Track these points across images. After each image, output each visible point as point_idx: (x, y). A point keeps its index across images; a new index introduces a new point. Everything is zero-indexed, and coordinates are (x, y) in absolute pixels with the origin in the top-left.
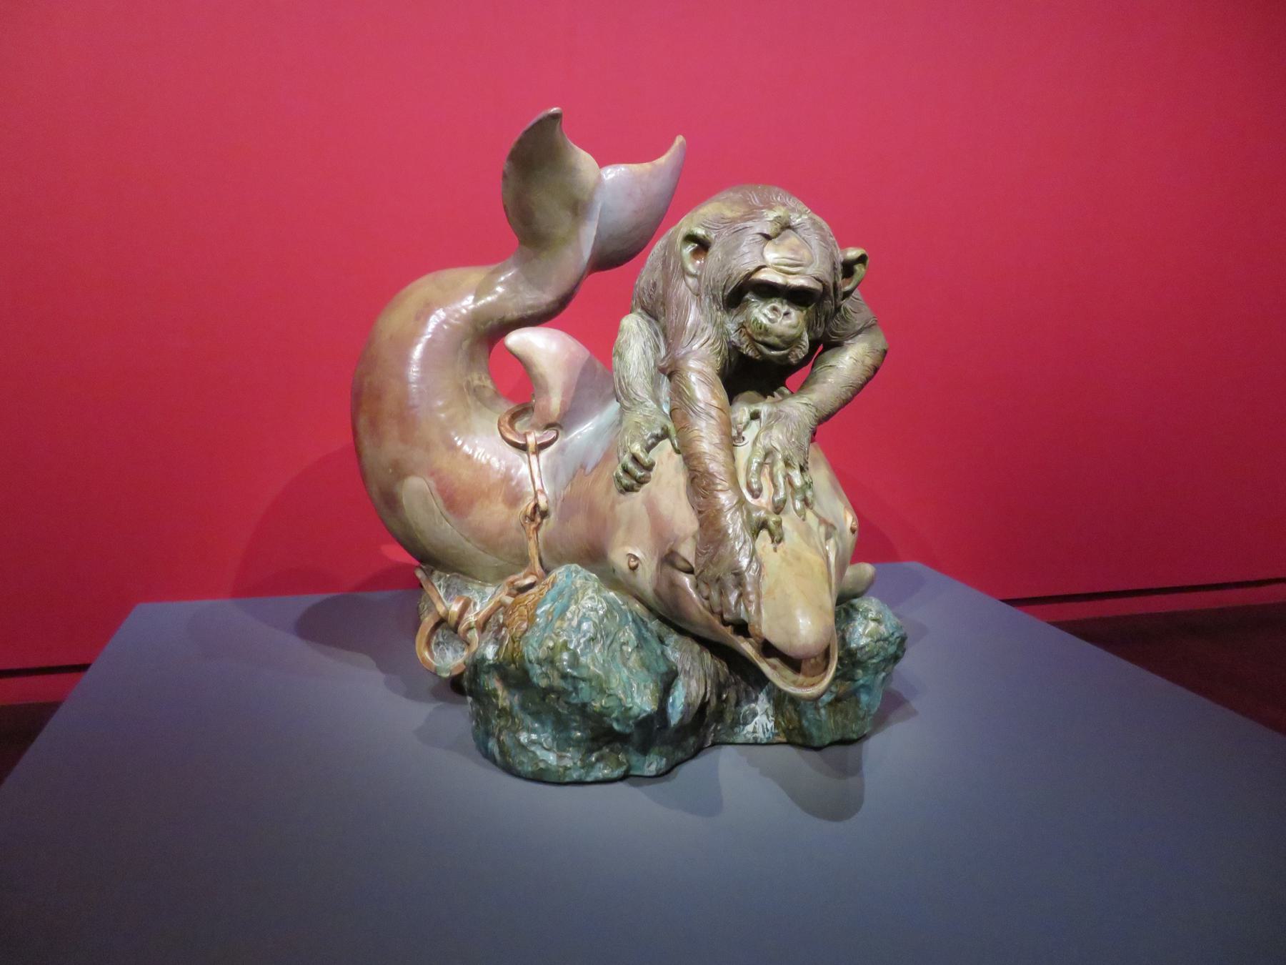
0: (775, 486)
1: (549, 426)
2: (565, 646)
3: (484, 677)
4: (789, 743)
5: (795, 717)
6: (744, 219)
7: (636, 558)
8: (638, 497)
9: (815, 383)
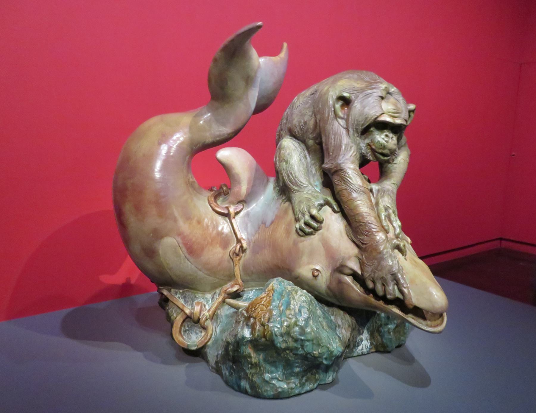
1: (240, 202)
2: (296, 324)
3: (243, 348)
4: (377, 351)
5: (379, 338)
6: (367, 88)
8: (315, 239)
9: (391, 172)
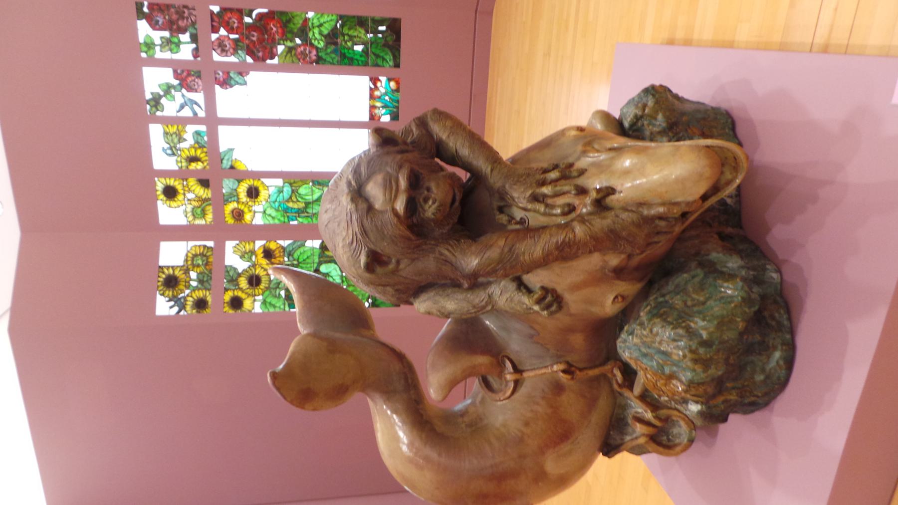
0: (564, 193)
7: (616, 297)
8: (568, 297)
